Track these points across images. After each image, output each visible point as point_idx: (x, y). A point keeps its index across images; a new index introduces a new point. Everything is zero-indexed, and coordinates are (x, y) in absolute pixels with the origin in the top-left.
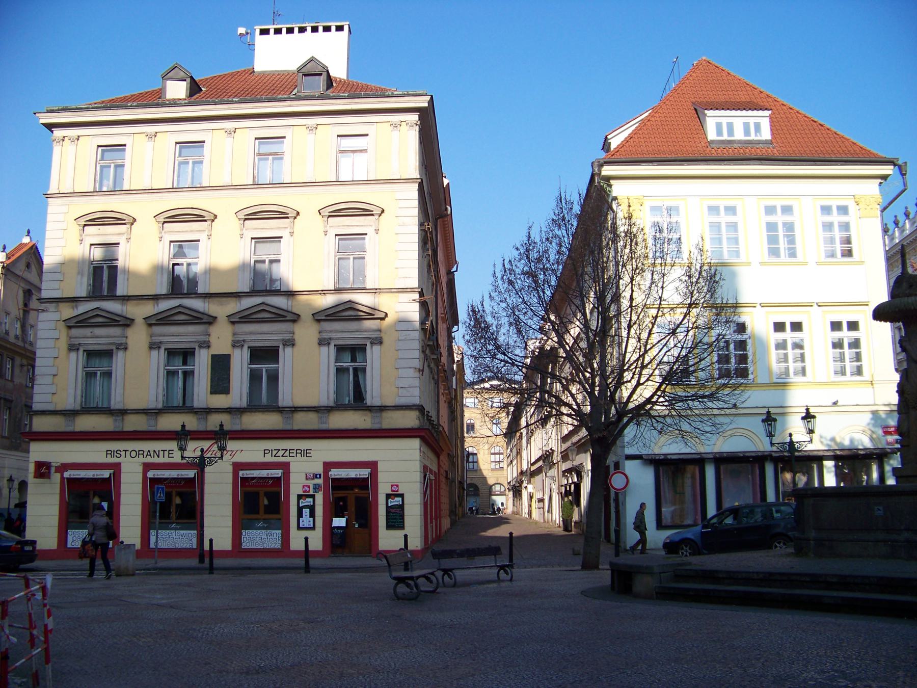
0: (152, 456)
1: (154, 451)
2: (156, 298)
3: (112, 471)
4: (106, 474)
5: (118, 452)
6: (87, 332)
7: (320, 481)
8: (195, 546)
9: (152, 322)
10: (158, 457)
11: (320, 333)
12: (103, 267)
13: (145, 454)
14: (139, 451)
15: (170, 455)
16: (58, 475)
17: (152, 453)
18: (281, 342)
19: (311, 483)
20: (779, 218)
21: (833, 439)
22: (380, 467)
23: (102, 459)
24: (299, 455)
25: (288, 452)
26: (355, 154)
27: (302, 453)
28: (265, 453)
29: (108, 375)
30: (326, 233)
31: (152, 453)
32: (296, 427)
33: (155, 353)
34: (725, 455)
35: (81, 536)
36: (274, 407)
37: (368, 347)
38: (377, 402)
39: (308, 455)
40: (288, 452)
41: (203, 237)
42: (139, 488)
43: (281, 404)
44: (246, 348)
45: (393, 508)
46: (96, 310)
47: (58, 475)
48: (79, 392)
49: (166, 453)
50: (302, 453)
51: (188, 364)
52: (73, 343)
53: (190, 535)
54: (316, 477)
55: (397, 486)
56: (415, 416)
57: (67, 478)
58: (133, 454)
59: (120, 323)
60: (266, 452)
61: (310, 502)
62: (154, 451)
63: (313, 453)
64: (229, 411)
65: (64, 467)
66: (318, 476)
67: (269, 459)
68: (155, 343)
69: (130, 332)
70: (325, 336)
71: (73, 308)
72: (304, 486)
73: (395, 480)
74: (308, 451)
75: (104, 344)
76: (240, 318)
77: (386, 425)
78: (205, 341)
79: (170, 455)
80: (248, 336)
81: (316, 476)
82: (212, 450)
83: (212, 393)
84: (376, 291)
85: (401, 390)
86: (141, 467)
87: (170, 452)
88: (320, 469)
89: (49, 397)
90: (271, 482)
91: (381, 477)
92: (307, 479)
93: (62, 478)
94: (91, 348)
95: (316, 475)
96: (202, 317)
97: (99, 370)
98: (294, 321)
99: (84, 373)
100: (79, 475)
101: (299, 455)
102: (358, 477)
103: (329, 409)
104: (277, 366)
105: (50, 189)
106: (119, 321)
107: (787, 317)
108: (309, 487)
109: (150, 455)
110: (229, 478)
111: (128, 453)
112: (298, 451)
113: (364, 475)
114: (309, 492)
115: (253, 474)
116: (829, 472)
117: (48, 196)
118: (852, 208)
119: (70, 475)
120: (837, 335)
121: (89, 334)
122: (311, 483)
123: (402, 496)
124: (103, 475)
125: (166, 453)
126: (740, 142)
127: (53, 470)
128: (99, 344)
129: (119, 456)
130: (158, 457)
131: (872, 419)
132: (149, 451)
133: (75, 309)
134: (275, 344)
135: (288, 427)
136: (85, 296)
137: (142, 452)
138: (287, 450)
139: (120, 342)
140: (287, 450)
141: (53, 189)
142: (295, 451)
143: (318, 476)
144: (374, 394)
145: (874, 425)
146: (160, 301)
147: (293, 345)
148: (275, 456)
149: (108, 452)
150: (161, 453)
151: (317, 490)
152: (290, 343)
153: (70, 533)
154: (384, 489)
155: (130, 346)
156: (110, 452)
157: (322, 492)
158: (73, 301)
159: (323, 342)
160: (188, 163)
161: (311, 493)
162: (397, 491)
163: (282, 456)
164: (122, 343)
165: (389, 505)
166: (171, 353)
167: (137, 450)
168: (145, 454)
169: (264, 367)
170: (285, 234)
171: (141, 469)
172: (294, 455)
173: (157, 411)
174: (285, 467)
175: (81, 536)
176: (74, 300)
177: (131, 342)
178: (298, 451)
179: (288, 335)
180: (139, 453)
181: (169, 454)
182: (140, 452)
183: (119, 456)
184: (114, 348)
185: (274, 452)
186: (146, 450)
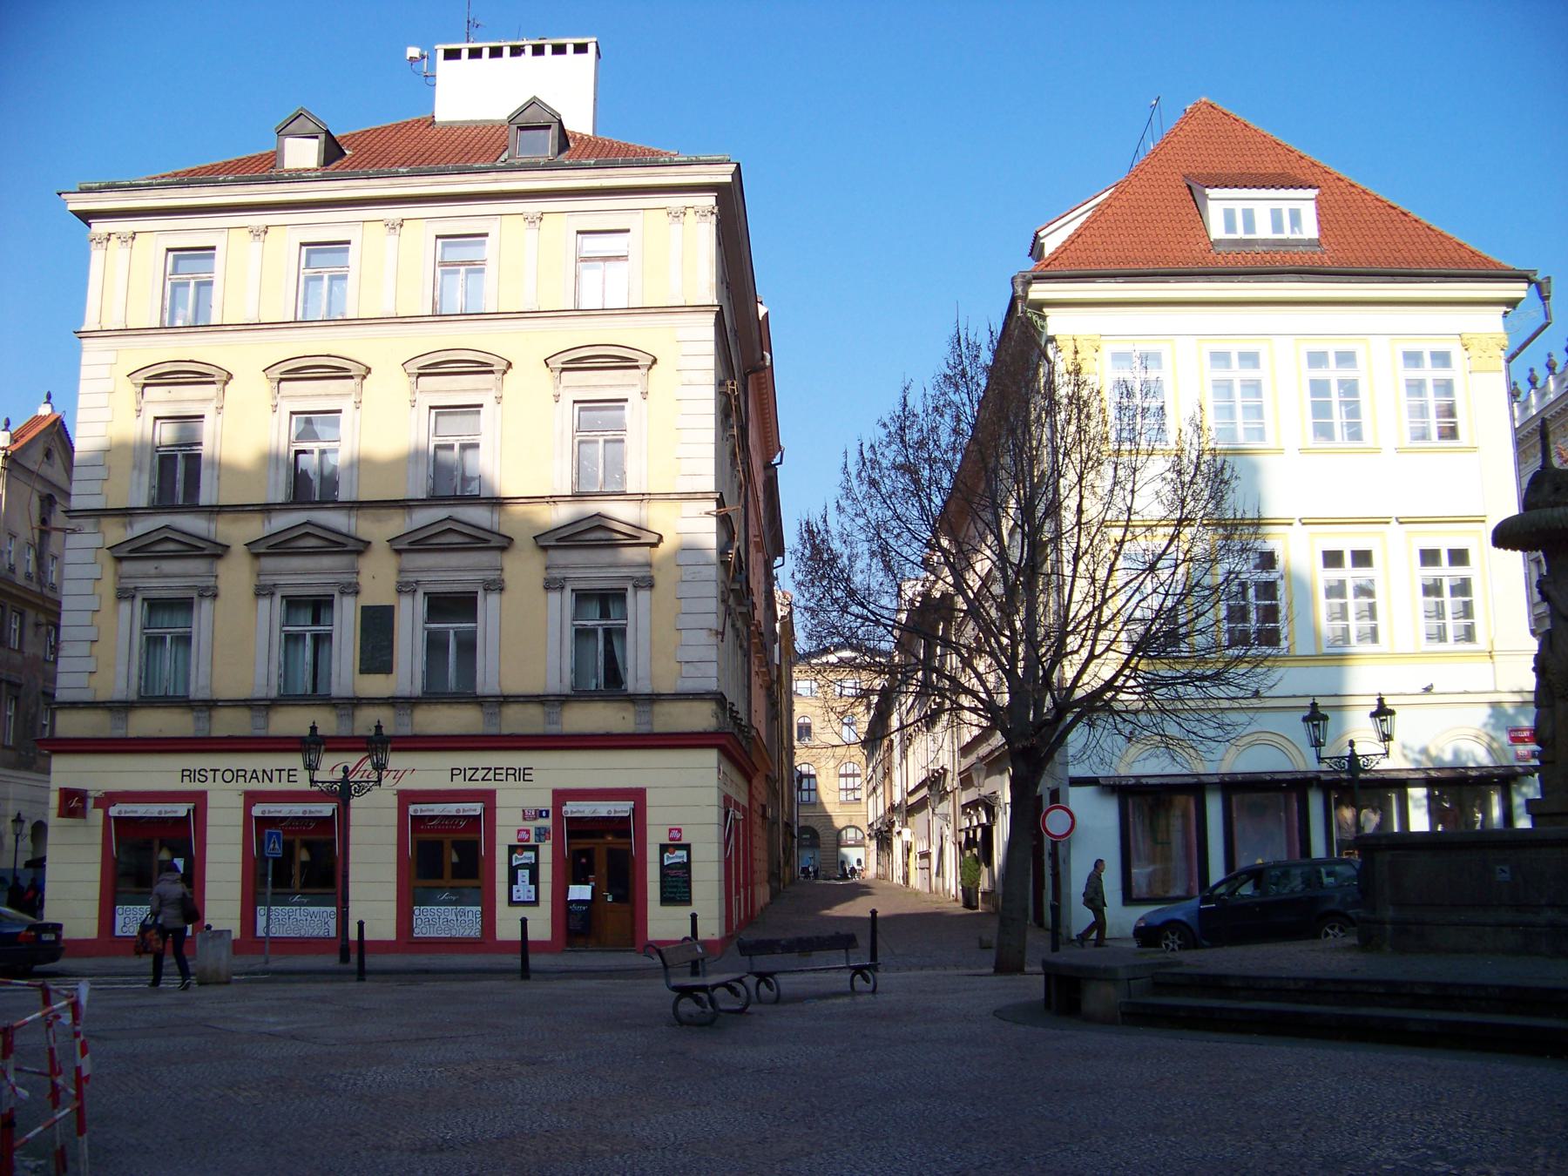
0: (261, 780)
1: (264, 771)
2: (266, 509)
3: (191, 805)
4: (181, 810)
5: (202, 773)
6: (149, 567)
7: (547, 823)
8: (333, 934)
9: (260, 550)
10: (271, 780)
11: (546, 568)
12: (176, 456)
13: (248, 777)
14: (238, 771)
15: (291, 779)
16: (100, 812)
17: (260, 775)
18: (481, 585)
19: (532, 825)
20: (1332, 373)
21: (1424, 751)
22: (650, 799)
23: (175, 784)
24: (511, 778)
25: (492, 772)
26: (607, 264)
27: (517, 774)
28: (452, 775)
29: (185, 640)
30: (557, 398)
31: (260, 775)
32: (506, 731)
33: (264, 603)
34: (1240, 777)
35: (138, 916)
36: (468, 697)
37: (630, 593)
38: (645, 688)
39: (526, 777)
40: (492, 772)
41: (347, 405)
42: (237, 834)
43: (480, 690)
44: (420, 595)
45: (673, 869)
46: (165, 530)
47: (100, 812)
48: (135, 671)
49: (284, 774)
50: (517, 774)
51: (322, 622)
52: (126, 586)
53: (325, 914)
54: (541, 816)
55: (680, 831)
56: (709, 712)
57: (115, 818)
58: (228, 776)
59: (206, 552)
60: (455, 772)
61: (530, 858)
62: (264, 771)
63: (535, 775)
64: (392, 702)
65: (110, 799)
66: (544, 814)
67: (460, 784)
68: (264, 587)
69: (222, 567)
70: (556, 574)
71: (125, 526)
72: (519, 831)
73: (675, 821)
74: (526, 772)
75: (178, 588)
76: (410, 543)
77: (659, 726)
78: (350, 584)
79: (291, 779)
80: (424, 574)
81: (540, 814)
82: (363, 768)
83: (362, 672)
84: (643, 497)
85: (685, 667)
86: (242, 799)
87: (291, 773)
88: (546, 802)
89: (83, 679)
90: (463, 824)
91: (652, 816)
92: (524, 819)
93: (107, 817)
94: (155, 594)
95: (541, 812)
96: (345, 542)
97: (170, 633)
98: (503, 549)
99: (144, 637)
100: (136, 812)
101: (511, 778)
102: (612, 815)
103: (562, 700)
104: (473, 625)
105: (86, 323)
106: (203, 549)
107: (1346, 542)
108: (528, 832)
109: (257, 778)
110: (392, 817)
111: (219, 774)
112: (509, 772)
113: (622, 811)
114: (528, 840)
115: (433, 810)
116: (1417, 807)
117: (81, 335)
118: (1457, 355)
119: (120, 812)
120: (1432, 572)
121: (153, 572)
122: (532, 825)
123: (687, 847)
124: (176, 812)
125: (284, 774)
126: (1265, 242)
127: (91, 803)
128: (170, 588)
129: (203, 779)
130: (271, 780)
131: (1491, 716)
132: (255, 771)
133: (129, 529)
134: (471, 588)
135: (493, 730)
136: (145, 506)
137: (243, 773)
138: (490, 769)
139: (204, 585)
140: (490, 769)
141: (90, 324)
142: (504, 772)
143: (544, 814)
144: (640, 673)
145: (1495, 727)
146: (273, 515)
147: (502, 590)
148: (470, 780)
149: (185, 773)
150: (276, 774)
151: (543, 838)
152: (496, 586)
153: (120, 911)
154: (656, 836)
155: (222, 592)
156: (188, 773)
157: (550, 842)
158: (124, 515)
159: (552, 585)
160: (321, 278)
161: (532, 842)
162: (680, 839)
163: (483, 779)
164: (208, 587)
165: (666, 863)
166: (293, 604)
167: (234, 770)
168: (248, 777)
169: (452, 627)
170: (487, 400)
171: (240, 801)
172: (503, 777)
173: (268, 703)
174: (488, 798)
175: (138, 916)
176: (127, 513)
177: (223, 585)
178: (509, 772)
179: (493, 573)
180: (237, 774)
181: (289, 775)
182: (240, 773)
183: (203, 779)
184: (195, 595)
185: (469, 773)
186: (250, 769)
